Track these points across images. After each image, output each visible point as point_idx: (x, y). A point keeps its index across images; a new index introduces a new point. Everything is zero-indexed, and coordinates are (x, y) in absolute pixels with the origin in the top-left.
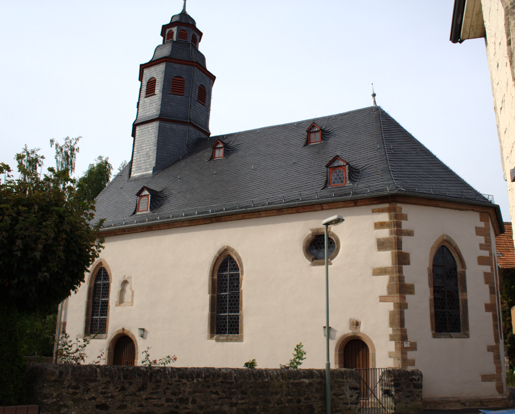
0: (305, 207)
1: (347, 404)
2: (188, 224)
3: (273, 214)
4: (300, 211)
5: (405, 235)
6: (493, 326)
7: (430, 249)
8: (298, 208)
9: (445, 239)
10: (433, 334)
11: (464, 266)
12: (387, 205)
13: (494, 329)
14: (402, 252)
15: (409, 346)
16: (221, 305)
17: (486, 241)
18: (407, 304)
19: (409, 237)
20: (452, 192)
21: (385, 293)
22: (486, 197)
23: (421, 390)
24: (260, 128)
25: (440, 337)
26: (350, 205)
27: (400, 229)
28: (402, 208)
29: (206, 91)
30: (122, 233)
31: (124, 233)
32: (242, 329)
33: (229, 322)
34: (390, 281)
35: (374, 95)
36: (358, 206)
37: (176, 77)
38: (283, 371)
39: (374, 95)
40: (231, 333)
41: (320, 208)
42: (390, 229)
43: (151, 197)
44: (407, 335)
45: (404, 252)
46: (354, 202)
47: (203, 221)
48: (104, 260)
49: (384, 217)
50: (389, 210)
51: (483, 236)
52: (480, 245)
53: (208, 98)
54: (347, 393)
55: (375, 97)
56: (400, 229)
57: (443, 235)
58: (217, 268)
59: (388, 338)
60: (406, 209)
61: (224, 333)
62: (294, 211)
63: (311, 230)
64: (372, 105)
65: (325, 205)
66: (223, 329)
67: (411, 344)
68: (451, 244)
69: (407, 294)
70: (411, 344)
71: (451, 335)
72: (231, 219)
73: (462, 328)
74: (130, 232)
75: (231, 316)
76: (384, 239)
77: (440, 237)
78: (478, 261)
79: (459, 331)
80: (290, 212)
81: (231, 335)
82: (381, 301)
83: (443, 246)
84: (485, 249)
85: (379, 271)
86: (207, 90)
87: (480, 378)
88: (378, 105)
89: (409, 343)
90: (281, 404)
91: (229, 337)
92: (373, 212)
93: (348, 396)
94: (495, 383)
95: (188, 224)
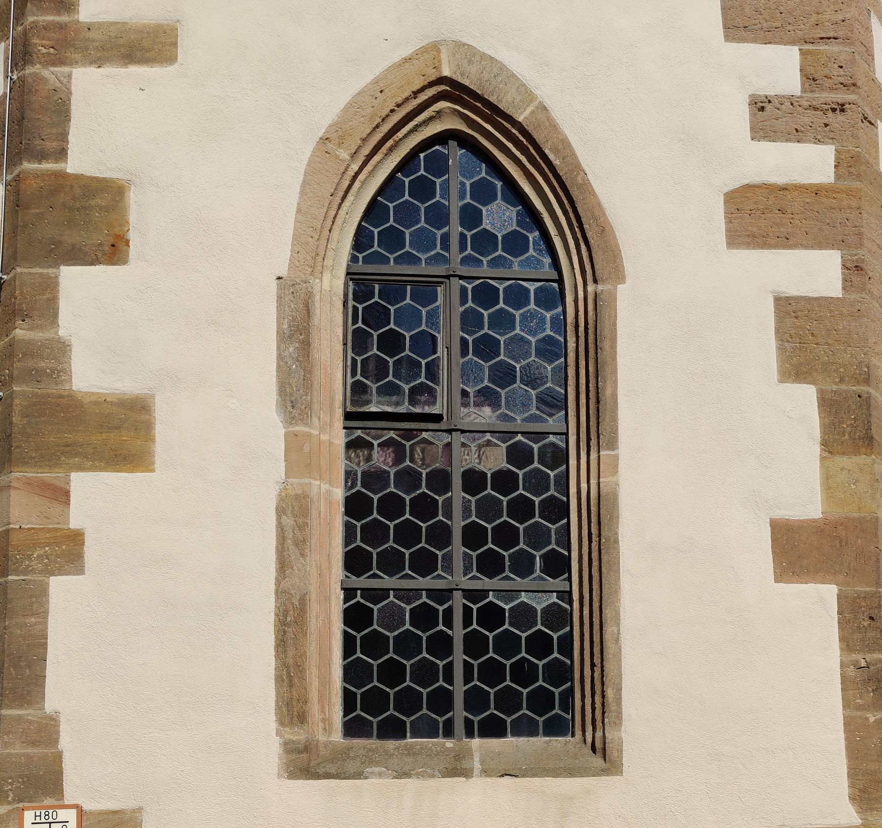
5: (99, 62)
6: (845, 680)
9: (446, 72)
13: (847, 704)
14: (61, 175)
17: (809, 79)
18: (77, 538)
19: (136, 70)
27: (64, 18)
38: (869, 451)
43: (564, 662)
44: (59, 757)
45: (78, 177)
51: (793, 43)
56: (64, 18)
69: (81, 468)
75: (491, 597)
77: (407, 60)
78: (729, 221)
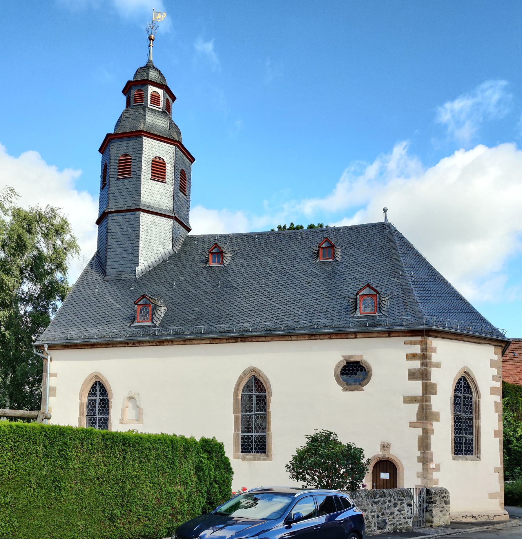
0: (339, 335)
1: (406, 518)
2: (209, 342)
3: (304, 339)
4: (332, 338)
5: (434, 367)
7: (453, 380)
8: (332, 335)
10: (453, 457)
11: (478, 395)
12: (419, 338)
15: (434, 467)
16: (103, 404)
20: (473, 328)
21: (415, 419)
22: (501, 331)
23: (449, 506)
24: (259, 233)
25: (458, 459)
26: (384, 335)
28: (433, 341)
29: (186, 177)
30: (123, 345)
31: (126, 345)
32: (271, 449)
33: (255, 442)
34: (419, 409)
35: (385, 210)
36: (391, 337)
37: (155, 157)
39: (385, 210)
40: (257, 452)
41: (354, 336)
42: (422, 361)
46: (388, 333)
47: (226, 340)
48: (98, 373)
49: (417, 349)
50: (421, 342)
52: (493, 376)
53: (188, 185)
54: (405, 509)
55: (387, 212)
57: (464, 367)
58: (241, 388)
59: (416, 460)
60: (435, 343)
61: (250, 452)
62: (327, 337)
63: (343, 356)
64: (383, 220)
65: (360, 334)
66: (248, 449)
67: (436, 465)
68: (469, 375)
70: (436, 465)
71: (466, 458)
72: (258, 340)
73: (474, 451)
74: (134, 345)
76: (415, 369)
79: (472, 454)
80: (322, 338)
81: (258, 454)
82: (410, 426)
83: (463, 377)
84: (496, 381)
85: (409, 399)
86: (187, 176)
87: (487, 496)
88: (389, 220)
89: (434, 464)
90: (368, 519)
91: (256, 457)
92: (405, 343)
93: (406, 511)
94: (499, 500)
95: (209, 342)
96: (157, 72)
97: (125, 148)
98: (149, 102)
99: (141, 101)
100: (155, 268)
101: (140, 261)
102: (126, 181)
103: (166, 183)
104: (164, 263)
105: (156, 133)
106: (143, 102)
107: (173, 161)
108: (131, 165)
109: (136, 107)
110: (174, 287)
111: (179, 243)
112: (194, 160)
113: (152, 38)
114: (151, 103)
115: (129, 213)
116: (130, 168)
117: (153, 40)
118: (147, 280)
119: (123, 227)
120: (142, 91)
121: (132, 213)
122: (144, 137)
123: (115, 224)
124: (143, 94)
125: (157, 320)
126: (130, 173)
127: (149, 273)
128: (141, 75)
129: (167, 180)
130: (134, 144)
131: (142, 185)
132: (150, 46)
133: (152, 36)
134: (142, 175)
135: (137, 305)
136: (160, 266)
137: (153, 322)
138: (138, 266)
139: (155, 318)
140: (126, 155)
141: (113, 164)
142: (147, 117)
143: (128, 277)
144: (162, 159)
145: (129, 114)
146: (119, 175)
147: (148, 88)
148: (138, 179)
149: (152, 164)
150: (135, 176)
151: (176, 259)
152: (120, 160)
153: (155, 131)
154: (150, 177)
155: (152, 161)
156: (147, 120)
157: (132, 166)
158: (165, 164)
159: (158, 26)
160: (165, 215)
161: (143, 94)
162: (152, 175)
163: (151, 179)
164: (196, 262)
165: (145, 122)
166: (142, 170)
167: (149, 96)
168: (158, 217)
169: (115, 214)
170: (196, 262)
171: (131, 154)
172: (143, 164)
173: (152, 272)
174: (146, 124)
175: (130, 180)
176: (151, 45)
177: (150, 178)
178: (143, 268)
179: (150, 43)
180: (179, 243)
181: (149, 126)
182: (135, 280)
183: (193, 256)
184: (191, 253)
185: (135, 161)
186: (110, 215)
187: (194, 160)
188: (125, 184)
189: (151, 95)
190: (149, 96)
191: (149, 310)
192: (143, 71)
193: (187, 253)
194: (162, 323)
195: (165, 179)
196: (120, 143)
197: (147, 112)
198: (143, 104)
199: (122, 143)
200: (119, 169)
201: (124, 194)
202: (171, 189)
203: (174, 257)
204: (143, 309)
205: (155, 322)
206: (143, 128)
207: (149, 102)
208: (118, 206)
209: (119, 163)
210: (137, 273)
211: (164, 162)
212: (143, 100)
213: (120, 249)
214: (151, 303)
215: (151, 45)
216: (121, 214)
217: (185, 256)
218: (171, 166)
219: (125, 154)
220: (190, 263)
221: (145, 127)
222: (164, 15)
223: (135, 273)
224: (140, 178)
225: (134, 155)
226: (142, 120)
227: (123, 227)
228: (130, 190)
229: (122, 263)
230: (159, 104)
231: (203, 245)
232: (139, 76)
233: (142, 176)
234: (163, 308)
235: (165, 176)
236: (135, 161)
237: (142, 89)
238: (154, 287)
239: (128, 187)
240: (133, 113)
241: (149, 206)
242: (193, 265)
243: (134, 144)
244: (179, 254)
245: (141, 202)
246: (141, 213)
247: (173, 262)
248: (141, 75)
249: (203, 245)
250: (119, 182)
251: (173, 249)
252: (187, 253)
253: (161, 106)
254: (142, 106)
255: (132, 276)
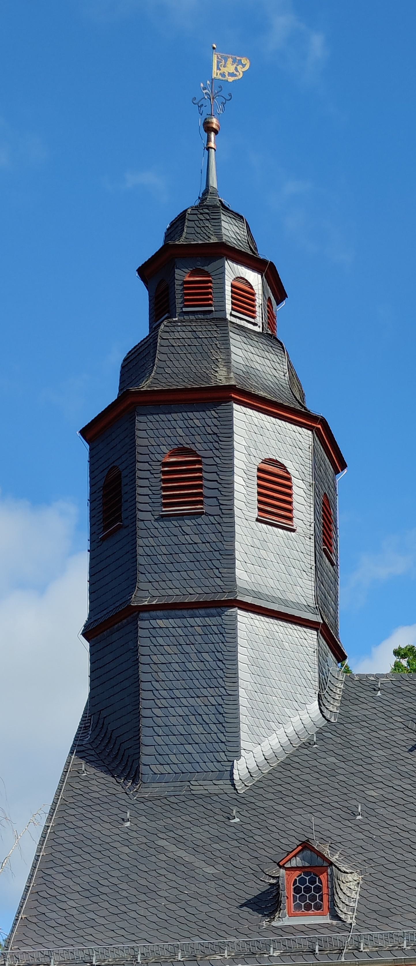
37: (265, 461)
96: (240, 224)
97: (180, 431)
98: (229, 307)
99: (206, 302)
100: (284, 765)
101: (243, 744)
102: (188, 522)
103: (294, 531)
104: (306, 751)
105: (262, 394)
106: (210, 305)
107: (308, 470)
108: (200, 478)
109: (192, 317)
110: (359, 817)
111: (333, 694)
112: (344, 466)
113: (214, 126)
114: (233, 309)
115: (202, 612)
116: (200, 486)
117: (216, 132)
118: (271, 796)
119: (187, 648)
120: (208, 274)
121: (213, 611)
122: (235, 406)
123: (161, 641)
124: (210, 282)
125: (345, 910)
126: (201, 502)
127: (270, 777)
128: (198, 230)
129: (296, 523)
130: (209, 421)
131: (237, 537)
132: (208, 148)
133: (214, 120)
134: (235, 509)
135: (287, 869)
136: (296, 759)
137: (335, 916)
138: (239, 757)
139: (341, 905)
140: (182, 451)
141: (147, 474)
142: (233, 348)
143: (213, 789)
144: (282, 465)
145: (177, 335)
146: (165, 505)
147: (223, 266)
148: (225, 520)
149: (259, 478)
150: (216, 511)
151: (339, 740)
152: (165, 464)
153: (258, 389)
154: (255, 514)
155: (259, 470)
156: (233, 356)
157: (204, 483)
158: (289, 479)
159: (230, 95)
160: (299, 618)
161: (210, 282)
162: (260, 509)
163: (257, 520)
164: (397, 750)
165: (228, 362)
166: (236, 495)
167: (228, 289)
168: (281, 623)
169: (159, 613)
170: (397, 750)
171: (198, 447)
172: (236, 478)
173: (278, 775)
174: (233, 369)
175: (199, 521)
176: (212, 144)
177: (256, 516)
178: (252, 766)
179: (209, 140)
180: (333, 694)
181: (241, 374)
182: (234, 796)
183: (382, 733)
184: (374, 723)
185: (214, 469)
186: (142, 615)
187: (344, 466)
188: (187, 529)
189: (232, 286)
190: (228, 289)
191: (320, 882)
192: (201, 217)
193: (364, 724)
194: (363, 918)
195: (290, 519)
196: (163, 416)
197: (231, 334)
198: (212, 311)
199: (169, 416)
200: (165, 489)
201: (183, 557)
202: (308, 548)
203: (329, 735)
204: (302, 881)
205: (343, 916)
206: (228, 378)
207: (229, 307)
208: (170, 592)
209: (164, 473)
210: (236, 777)
211: (288, 473)
212: (210, 299)
213: (180, 711)
214: (325, 864)
215: (212, 144)
216: (179, 613)
217: (359, 731)
218: (304, 486)
219: (179, 449)
220: (380, 752)
221: (232, 375)
222: (244, 66)
223: (232, 779)
224: (232, 516)
225: (209, 454)
226: (220, 357)
227: (187, 648)
228: (203, 547)
229: (189, 748)
230: (251, 313)
231: (402, 701)
232: (192, 230)
233: (237, 512)
234: (350, 877)
235: (290, 511)
236: (214, 469)
237: (206, 268)
238: (299, 818)
239: (196, 539)
240: (190, 335)
241: (257, 595)
242: (392, 758)
243: (209, 421)
244: (342, 727)
245: (239, 582)
246: (239, 612)
247: (331, 747)
248: (198, 230)
249: (402, 701)
250: (168, 524)
251: (322, 712)
252: (364, 724)
253: (259, 320)
254: (209, 316)
255: (224, 785)
